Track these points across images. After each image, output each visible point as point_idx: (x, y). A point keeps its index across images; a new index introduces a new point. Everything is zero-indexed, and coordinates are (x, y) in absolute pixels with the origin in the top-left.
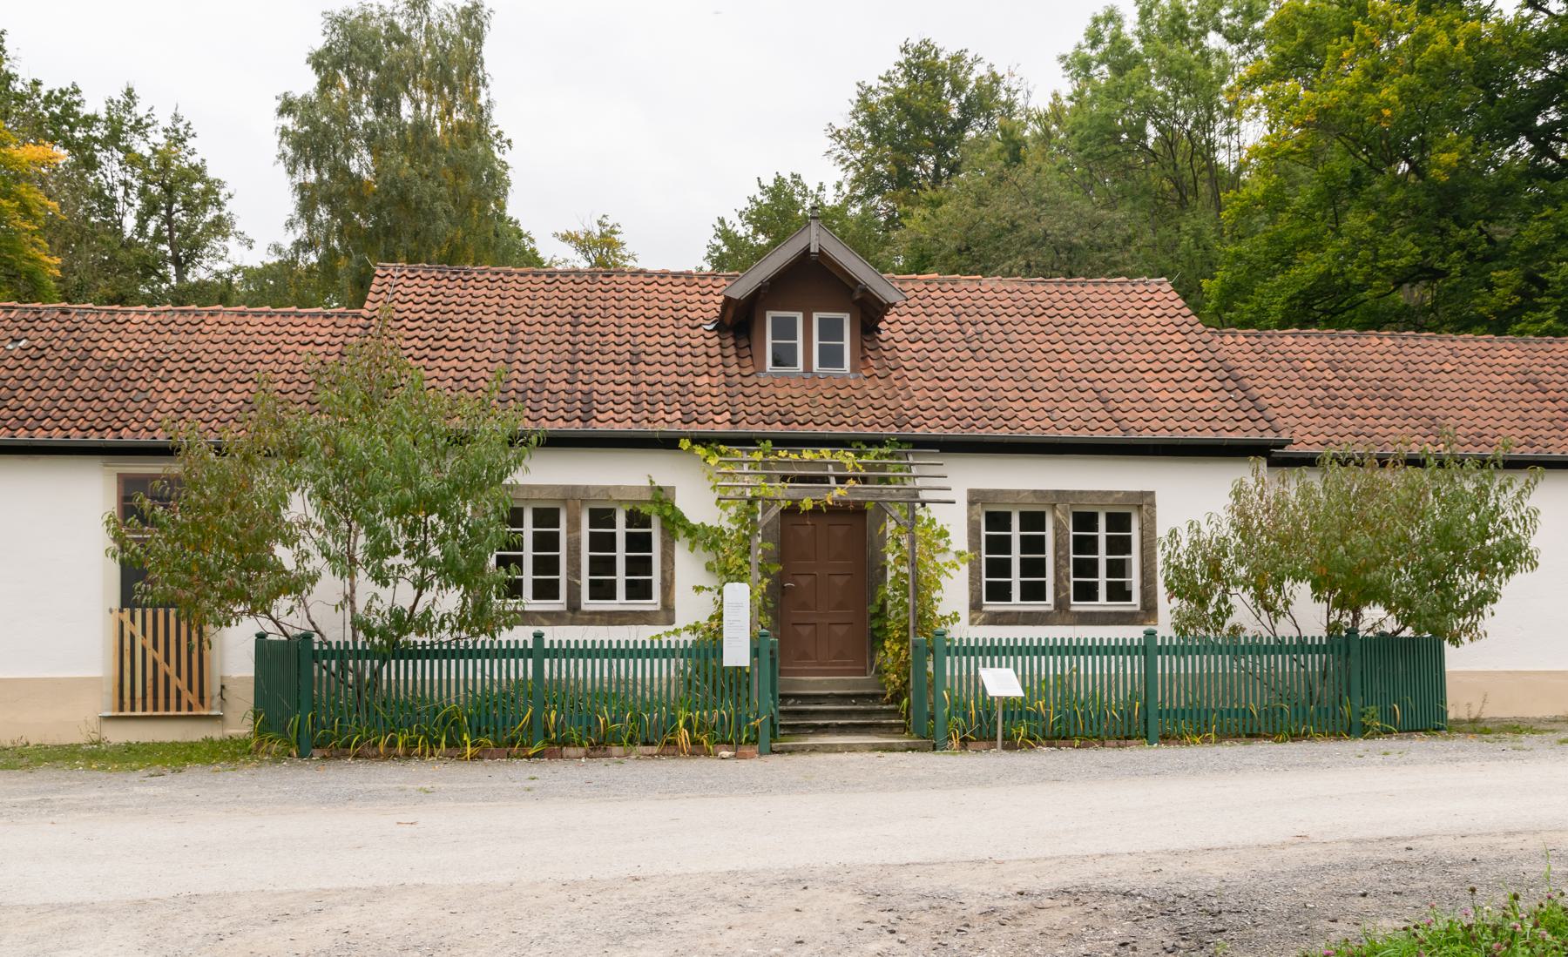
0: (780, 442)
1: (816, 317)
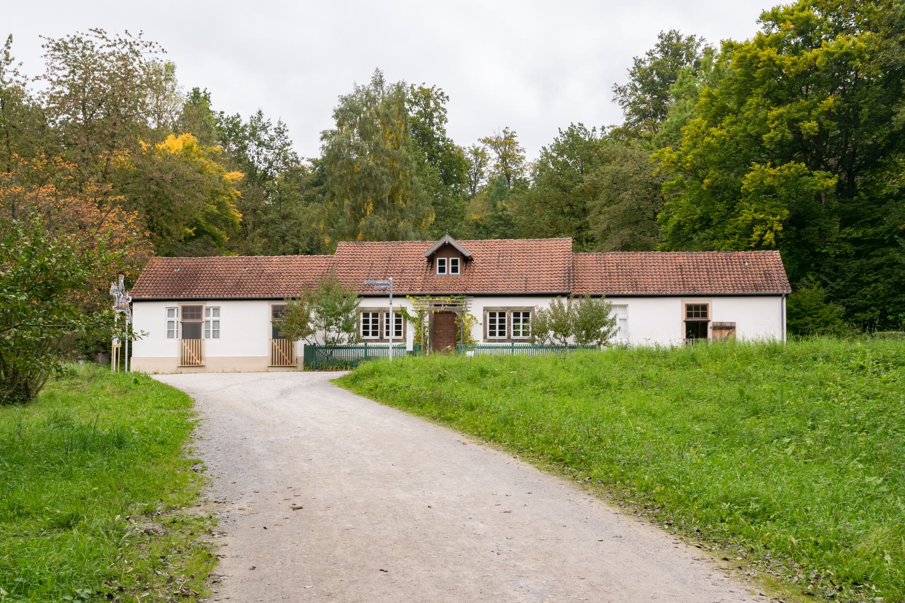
0: (433, 296)
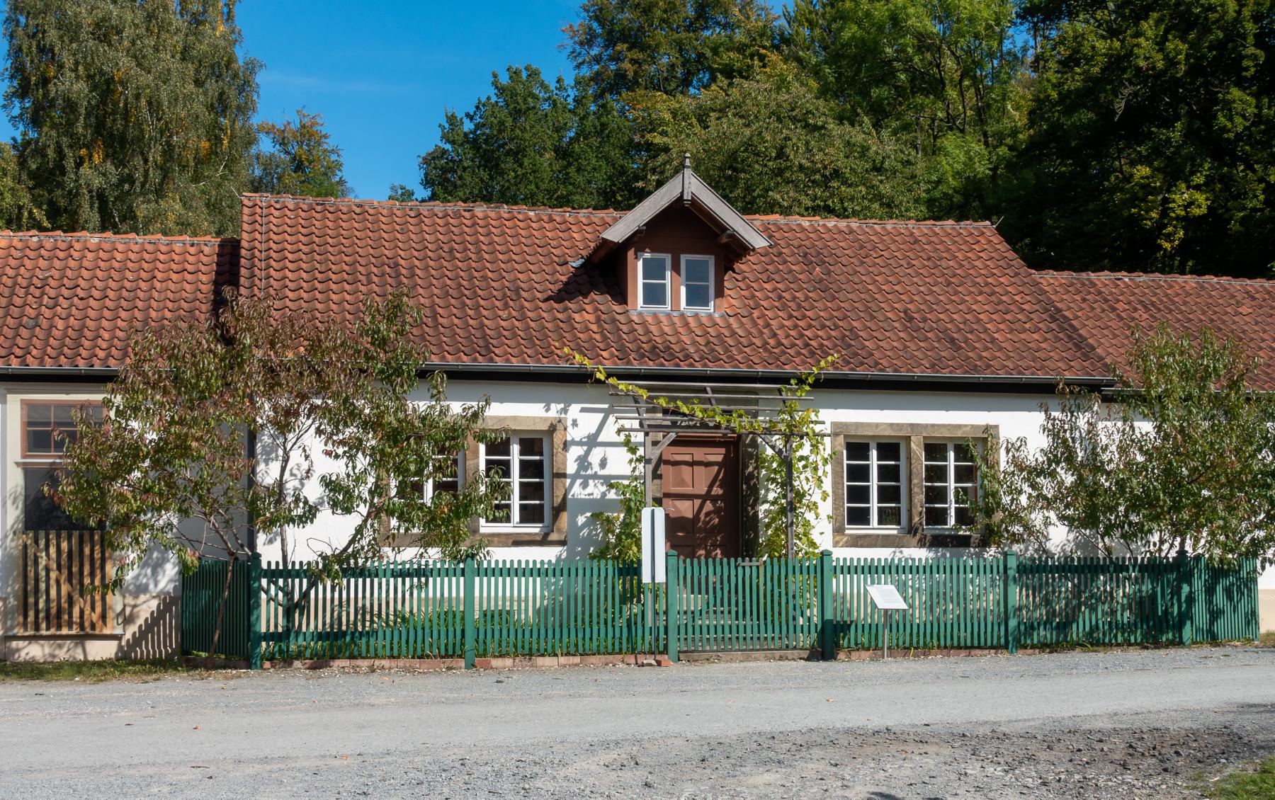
1: (684, 258)
